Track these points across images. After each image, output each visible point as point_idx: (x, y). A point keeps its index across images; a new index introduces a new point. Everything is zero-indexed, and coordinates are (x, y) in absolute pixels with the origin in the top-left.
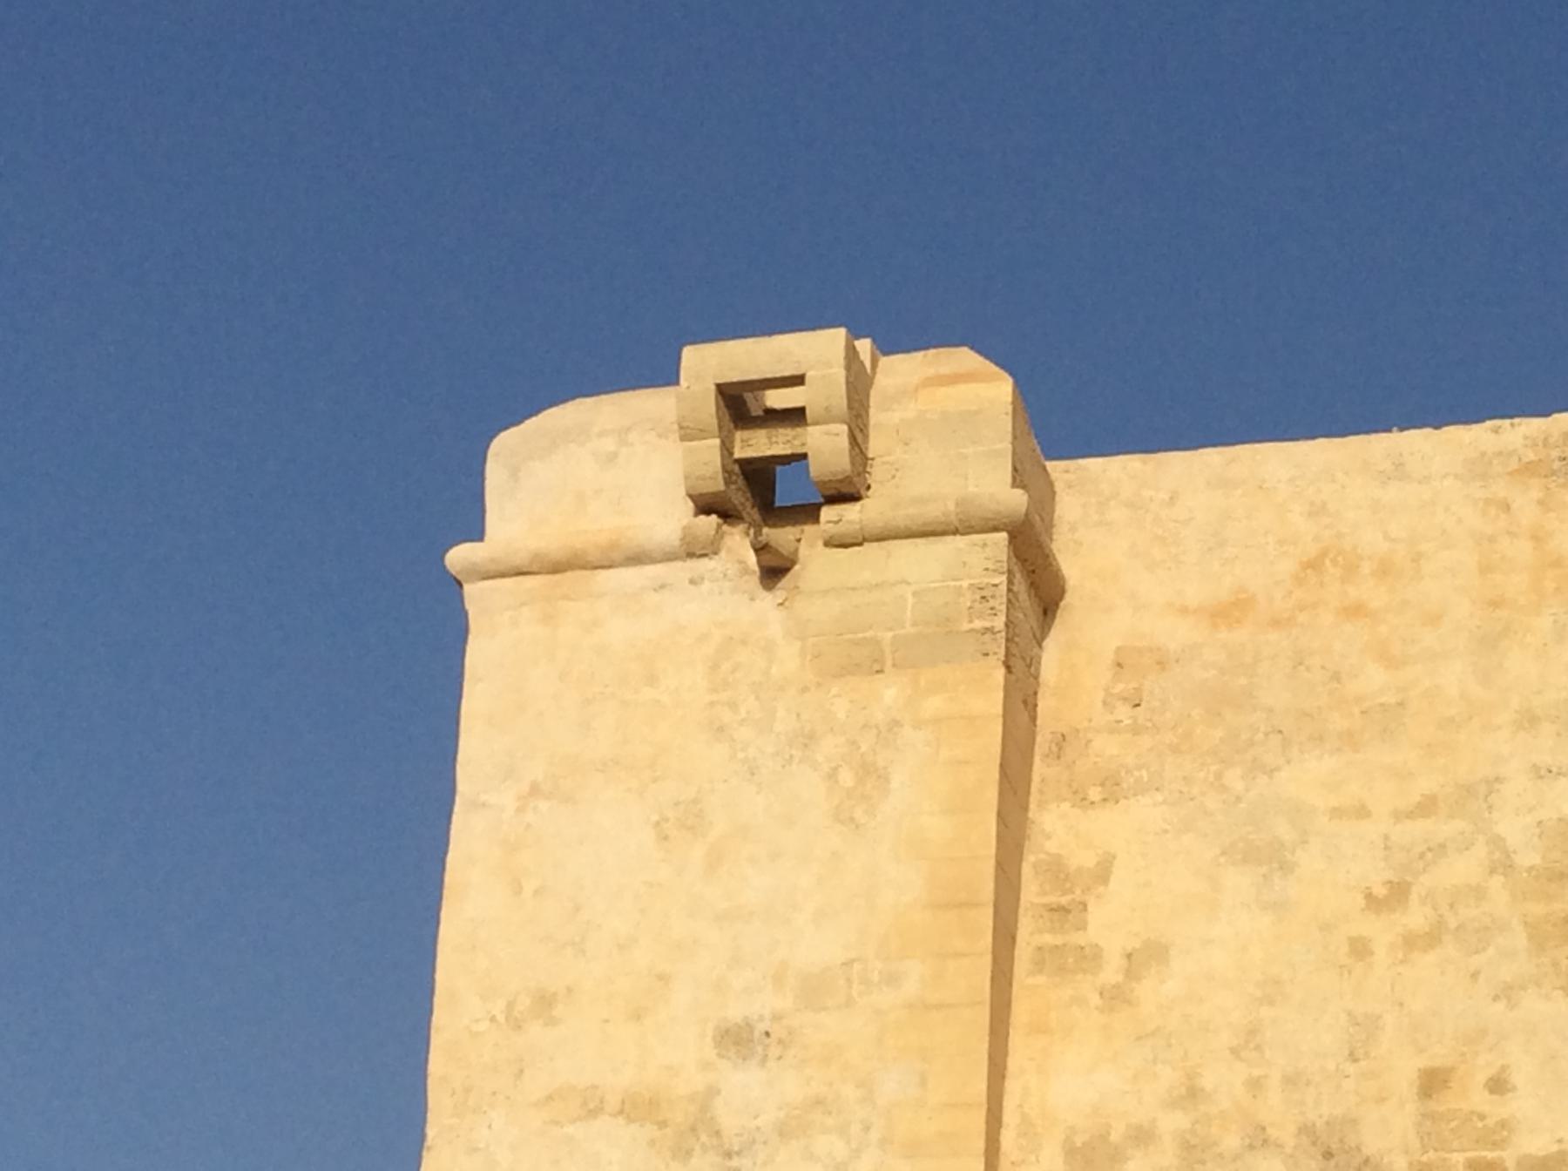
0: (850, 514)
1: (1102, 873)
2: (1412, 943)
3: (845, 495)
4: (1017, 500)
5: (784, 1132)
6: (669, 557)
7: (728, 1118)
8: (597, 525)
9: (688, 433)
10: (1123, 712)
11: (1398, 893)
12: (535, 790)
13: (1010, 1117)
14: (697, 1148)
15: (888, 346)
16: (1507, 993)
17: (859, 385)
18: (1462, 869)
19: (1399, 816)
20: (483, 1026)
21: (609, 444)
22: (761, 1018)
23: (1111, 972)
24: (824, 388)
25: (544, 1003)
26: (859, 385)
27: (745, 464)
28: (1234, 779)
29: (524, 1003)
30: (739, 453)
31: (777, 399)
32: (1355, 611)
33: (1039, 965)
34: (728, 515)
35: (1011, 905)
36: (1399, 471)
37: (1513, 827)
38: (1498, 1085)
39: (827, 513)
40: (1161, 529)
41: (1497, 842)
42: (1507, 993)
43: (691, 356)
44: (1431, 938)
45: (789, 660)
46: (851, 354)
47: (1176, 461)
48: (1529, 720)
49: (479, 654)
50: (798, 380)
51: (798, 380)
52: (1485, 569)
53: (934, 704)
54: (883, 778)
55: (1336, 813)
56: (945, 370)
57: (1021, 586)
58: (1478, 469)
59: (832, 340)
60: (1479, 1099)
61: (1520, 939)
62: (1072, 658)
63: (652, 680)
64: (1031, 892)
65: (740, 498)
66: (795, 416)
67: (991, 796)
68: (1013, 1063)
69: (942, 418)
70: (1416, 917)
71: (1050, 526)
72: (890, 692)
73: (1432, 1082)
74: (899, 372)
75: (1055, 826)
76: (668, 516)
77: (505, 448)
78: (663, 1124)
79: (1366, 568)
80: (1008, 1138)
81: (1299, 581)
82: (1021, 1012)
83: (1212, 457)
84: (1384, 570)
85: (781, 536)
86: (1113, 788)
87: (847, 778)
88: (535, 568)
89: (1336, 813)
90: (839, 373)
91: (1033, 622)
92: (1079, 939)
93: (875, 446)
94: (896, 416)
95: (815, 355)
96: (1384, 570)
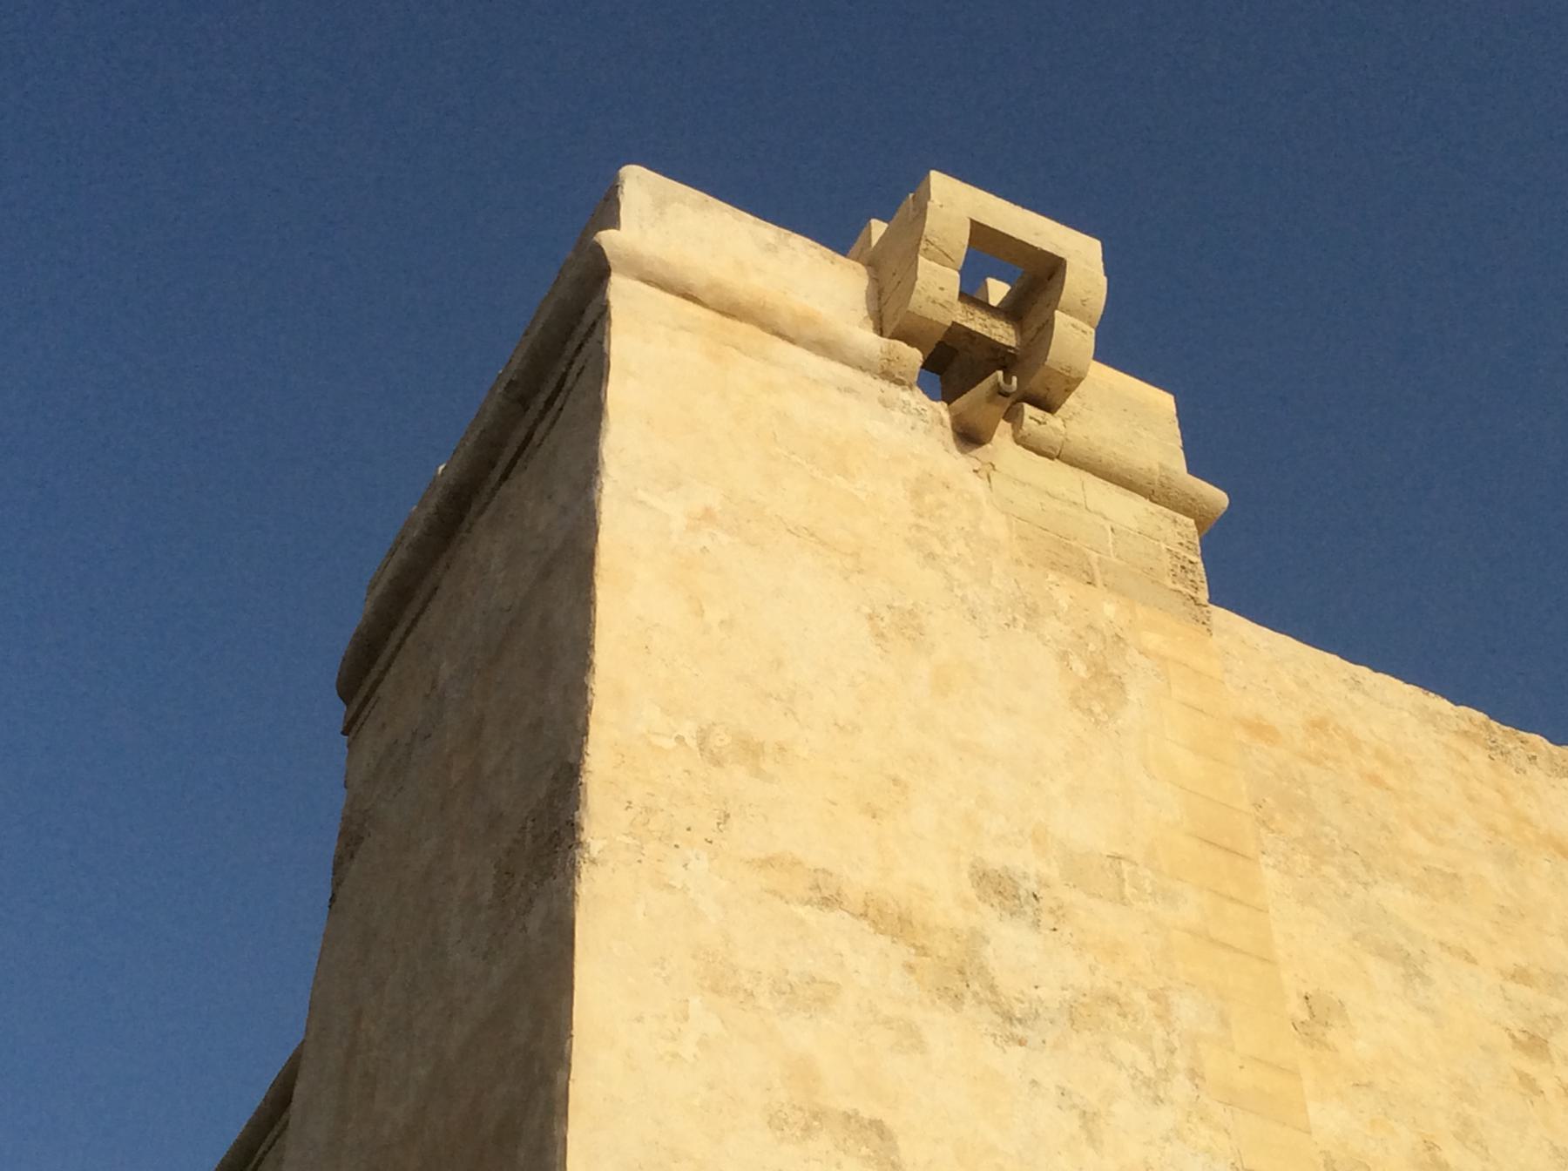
14: (969, 995)
20: (669, 744)
22: (1026, 877)
56: (541, 406)
78: (922, 951)
79: (952, 993)
88: (707, 298)
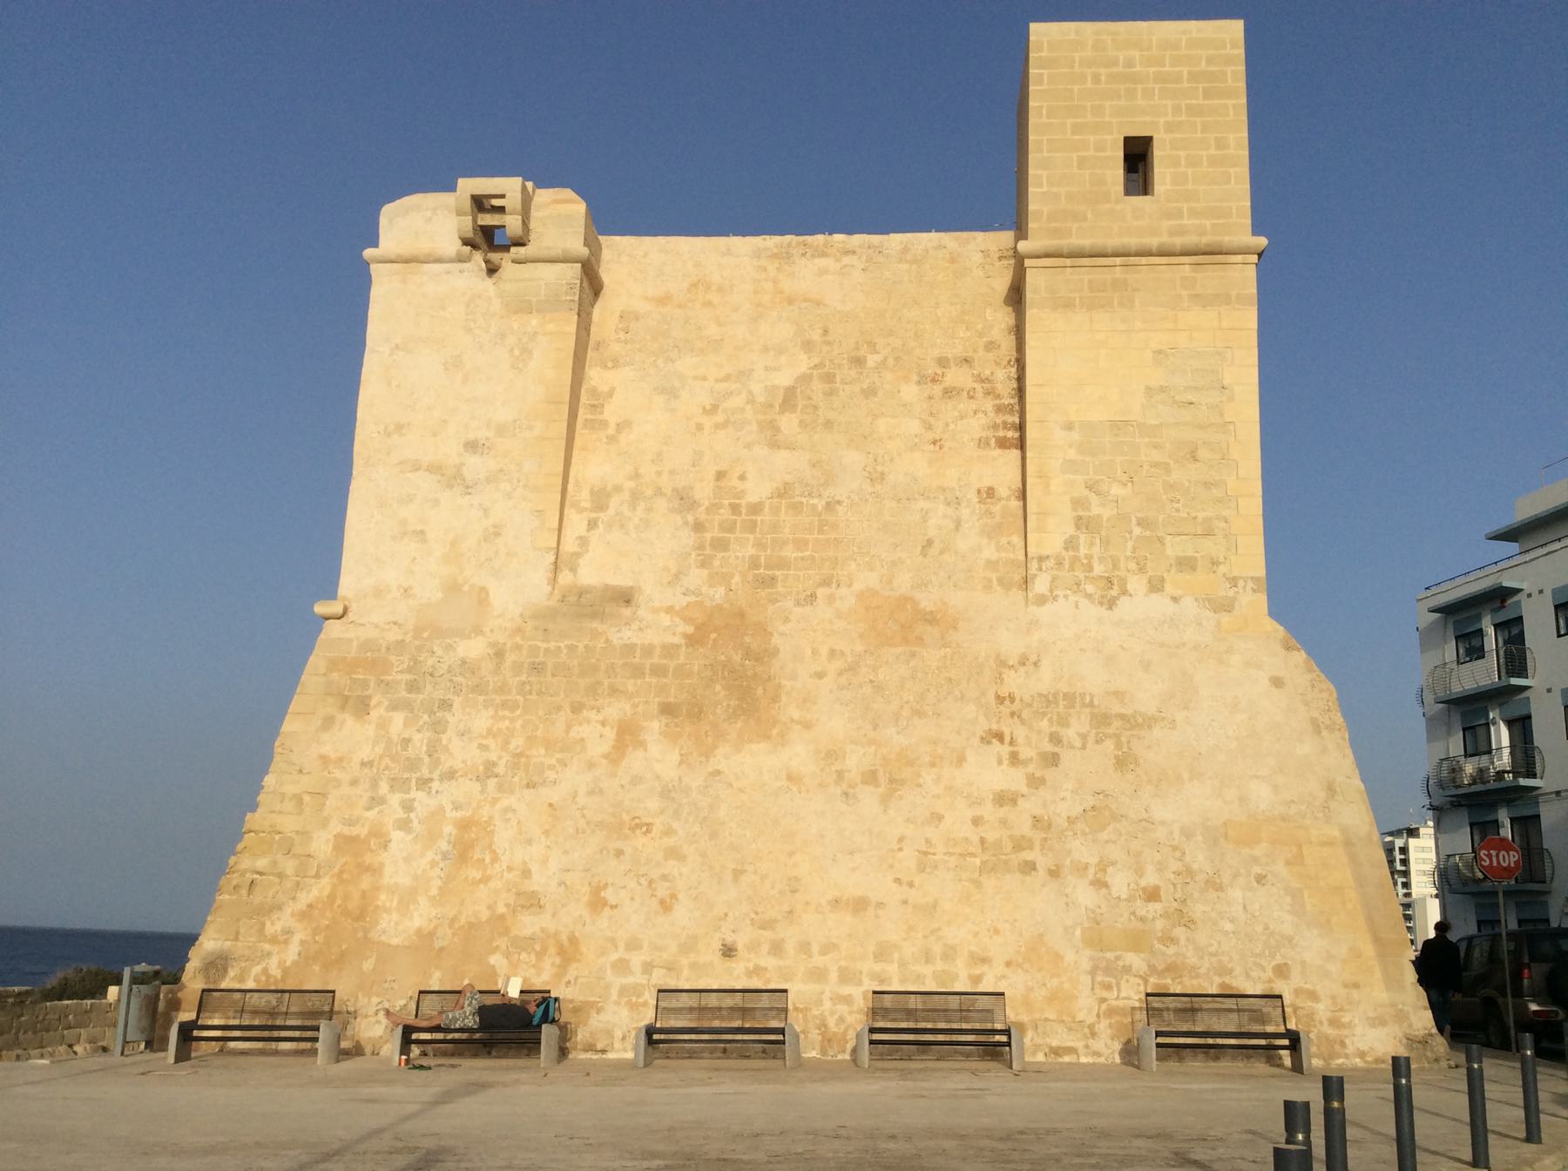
0: (521, 250)
1: (611, 394)
2: (717, 426)
3: (520, 243)
4: (585, 251)
5: (488, 480)
6: (451, 261)
7: (468, 474)
8: (424, 246)
9: (459, 213)
10: (622, 335)
11: (714, 409)
12: (397, 347)
13: (571, 480)
15: (541, 184)
16: (748, 446)
17: (527, 200)
18: (737, 401)
19: (717, 381)
21: (429, 214)
23: (611, 431)
24: (513, 200)
25: (399, 428)
26: (527, 200)
27: (482, 227)
28: (660, 362)
29: (392, 427)
30: (480, 222)
31: (496, 202)
32: (709, 304)
33: (585, 427)
34: (474, 246)
35: (575, 403)
36: (728, 252)
37: (756, 389)
38: (742, 478)
39: (513, 249)
40: (643, 265)
41: (750, 392)
42: (748, 446)
43: (461, 182)
44: (725, 425)
45: (496, 305)
46: (524, 188)
47: (648, 241)
48: (766, 349)
49: (375, 292)
50: (503, 196)
51: (503, 196)
52: (756, 292)
53: (551, 327)
54: (530, 353)
55: (695, 378)
57: (585, 284)
58: (757, 254)
59: (515, 182)
60: (735, 482)
61: (754, 427)
62: (604, 314)
63: (443, 308)
64: (584, 399)
65: (480, 240)
66: (501, 210)
67: (563, 454)
68: (574, 461)
69: (558, 216)
70: (720, 418)
71: (598, 261)
72: (534, 321)
73: (720, 475)
74: (543, 196)
75: (595, 376)
76: (450, 244)
77: (388, 211)
80: (570, 487)
81: (689, 290)
82: (578, 442)
83: (661, 240)
84: (720, 289)
85: (495, 257)
86: (616, 363)
87: (517, 352)
89: (695, 378)
90: (519, 196)
91: (591, 295)
92: (599, 417)
93: (532, 225)
94: (541, 214)
95: (509, 187)
96: (720, 289)
